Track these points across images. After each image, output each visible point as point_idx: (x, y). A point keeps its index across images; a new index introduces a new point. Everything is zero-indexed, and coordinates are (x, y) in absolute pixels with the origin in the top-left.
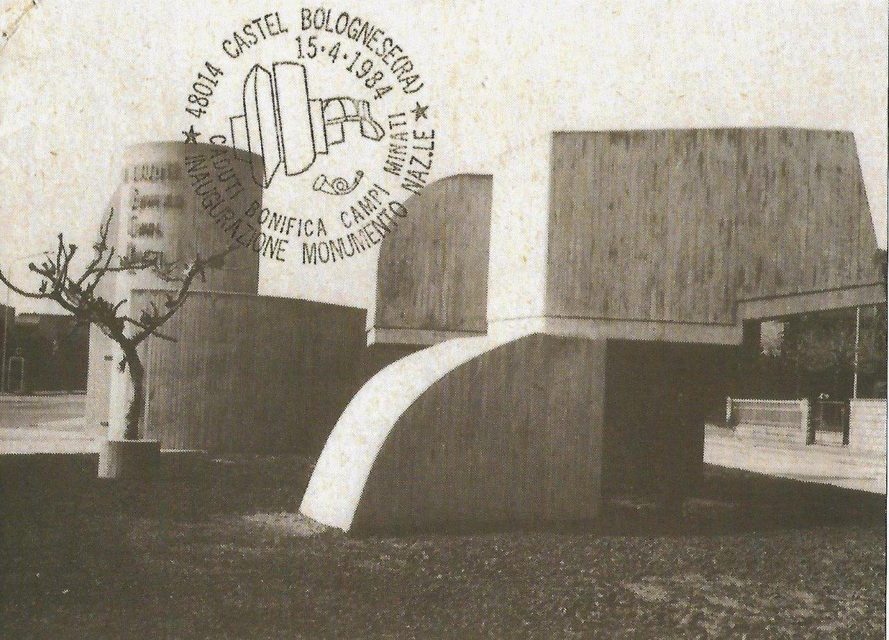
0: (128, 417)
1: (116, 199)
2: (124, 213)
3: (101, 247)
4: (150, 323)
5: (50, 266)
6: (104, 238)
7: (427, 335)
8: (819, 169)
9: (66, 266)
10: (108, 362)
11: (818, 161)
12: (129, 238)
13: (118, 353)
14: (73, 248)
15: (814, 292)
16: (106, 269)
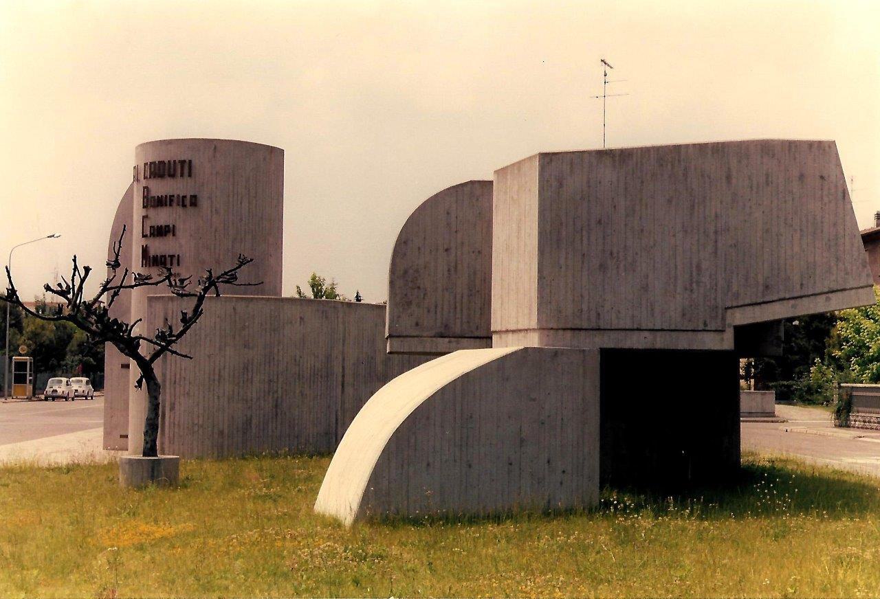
0: (146, 433)
1: (128, 195)
2: (138, 211)
3: (114, 265)
4: (165, 341)
5: (64, 286)
6: (117, 255)
7: (442, 343)
8: (802, 177)
9: (80, 288)
10: (124, 371)
11: (806, 169)
12: (144, 242)
13: (135, 371)
14: (87, 270)
15: (801, 297)
16: (121, 287)
